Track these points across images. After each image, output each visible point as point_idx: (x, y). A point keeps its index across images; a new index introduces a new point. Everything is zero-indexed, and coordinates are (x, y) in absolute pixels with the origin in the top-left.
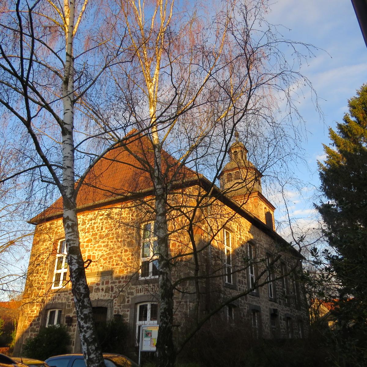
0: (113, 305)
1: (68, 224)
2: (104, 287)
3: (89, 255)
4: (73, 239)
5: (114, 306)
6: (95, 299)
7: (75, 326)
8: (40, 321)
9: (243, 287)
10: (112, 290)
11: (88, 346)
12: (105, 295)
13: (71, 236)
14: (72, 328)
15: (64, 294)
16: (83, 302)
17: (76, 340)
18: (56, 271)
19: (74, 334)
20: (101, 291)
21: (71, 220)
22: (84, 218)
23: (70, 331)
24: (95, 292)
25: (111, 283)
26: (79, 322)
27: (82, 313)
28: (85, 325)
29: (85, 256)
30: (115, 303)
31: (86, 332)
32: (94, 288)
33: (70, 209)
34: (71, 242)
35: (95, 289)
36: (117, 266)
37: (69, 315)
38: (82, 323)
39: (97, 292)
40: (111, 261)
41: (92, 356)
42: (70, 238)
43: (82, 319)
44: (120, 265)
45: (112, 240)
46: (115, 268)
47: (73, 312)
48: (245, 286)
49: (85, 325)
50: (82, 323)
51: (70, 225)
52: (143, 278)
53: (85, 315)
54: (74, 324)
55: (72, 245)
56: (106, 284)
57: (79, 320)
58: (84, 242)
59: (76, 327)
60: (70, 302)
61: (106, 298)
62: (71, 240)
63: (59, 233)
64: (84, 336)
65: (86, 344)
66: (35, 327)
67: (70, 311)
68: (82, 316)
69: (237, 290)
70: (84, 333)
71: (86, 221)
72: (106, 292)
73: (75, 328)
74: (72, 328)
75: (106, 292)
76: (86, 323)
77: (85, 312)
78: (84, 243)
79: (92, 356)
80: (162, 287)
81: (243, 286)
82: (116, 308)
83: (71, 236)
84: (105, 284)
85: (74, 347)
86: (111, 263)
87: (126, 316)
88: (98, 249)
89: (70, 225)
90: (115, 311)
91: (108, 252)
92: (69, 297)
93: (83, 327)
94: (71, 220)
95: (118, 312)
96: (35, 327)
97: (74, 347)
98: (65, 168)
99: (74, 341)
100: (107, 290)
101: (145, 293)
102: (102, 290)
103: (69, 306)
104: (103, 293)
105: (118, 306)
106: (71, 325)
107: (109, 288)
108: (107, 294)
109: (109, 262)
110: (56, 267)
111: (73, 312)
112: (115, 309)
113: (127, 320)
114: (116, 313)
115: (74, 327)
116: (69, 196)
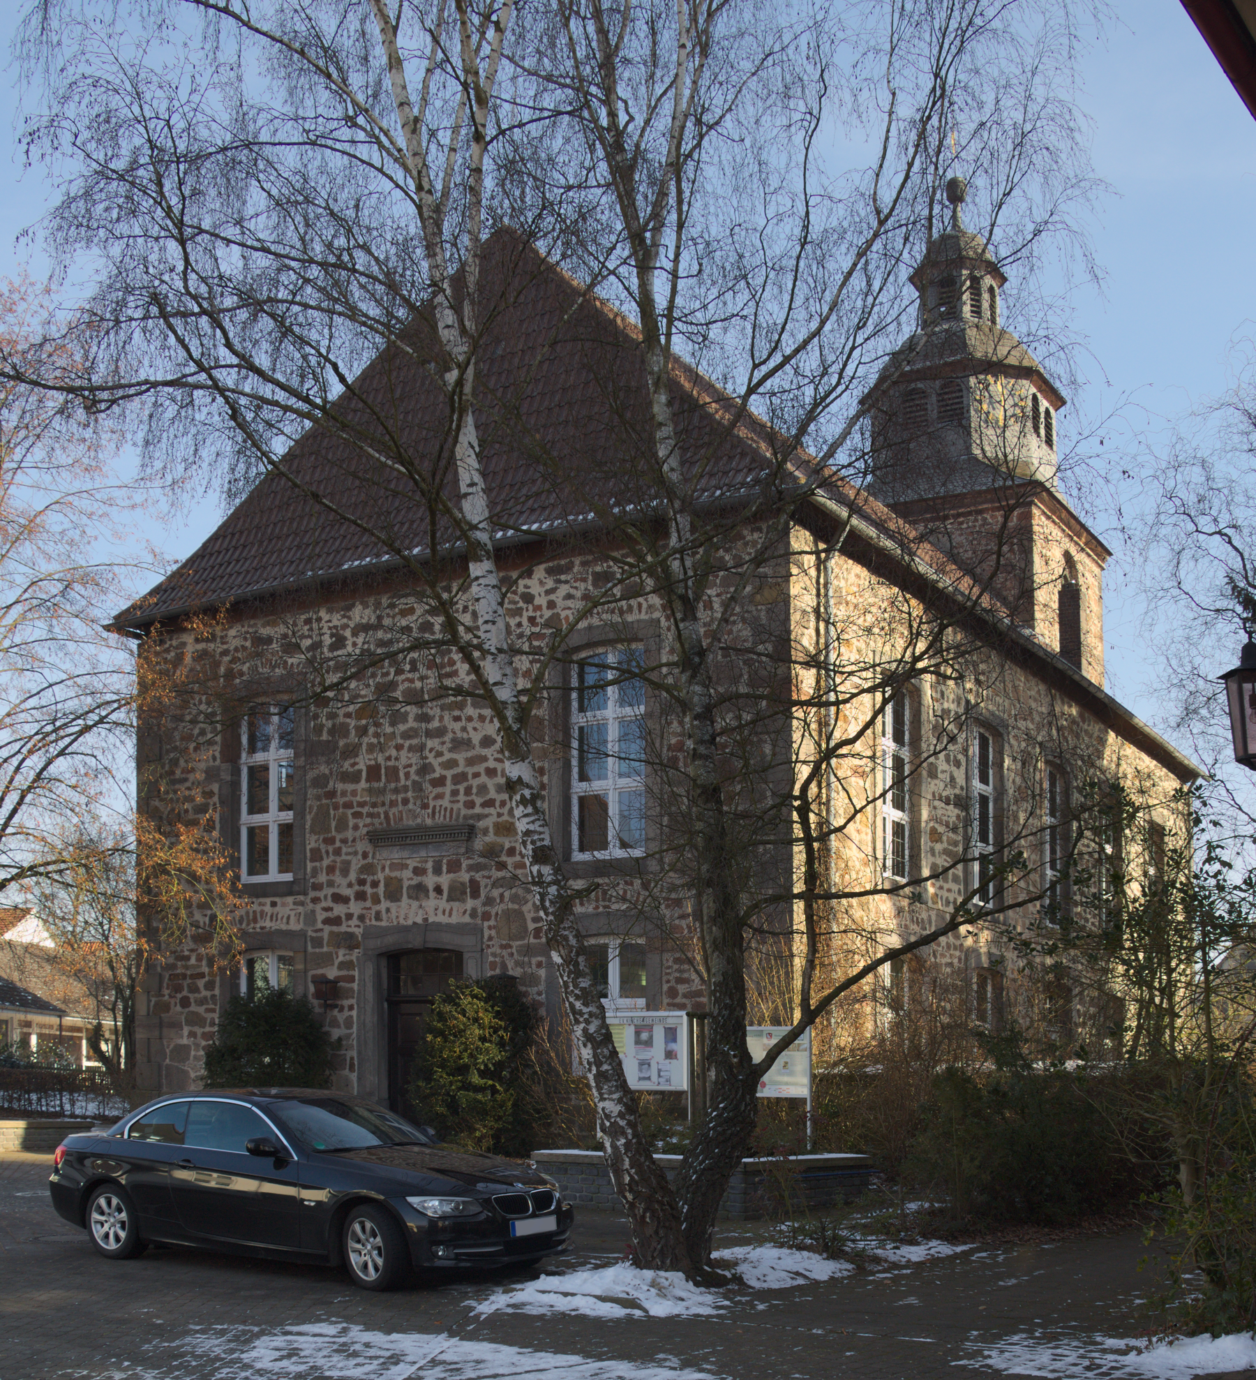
0: (482, 943)
1: (522, 796)
2: (445, 880)
3: (373, 762)
4: (538, 829)
5: (488, 946)
6: (415, 923)
7: (351, 1008)
8: (217, 992)
9: (949, 890)
10: (475, 894)
11: (594, 1048)
12: (451, 910)
13: (533, 822)
14: (341, 1017)
15: (295, 903)
16: (577, 964)
17: (359, 1053)
18: (247, 819)
19: (349, 1036)
20: (432, 894)
21: (528, 786)
22: (337, 620)
23: (334, 1023)
24: (410, 897)
25: (471, 868)
26: (571, 1004)
27: (576, 986)
28: (585, 1010)
29: (356, 767)
30: (490, 938)
31: (587, 1022)
32: (406, 884)
33: (523, 760)
34: (536, 837)
35: (409, 887)
36: (487, 810)
37: (320, 971)
38: (578, 1005)
39: (417, 899)
40: (461, 788)
41: (605, 1067)
42: (531, 827)
43: (577, 998)
44: (497, 804)
45: (456, 713)
46: (480, 817)
47: (336, 963)
48: (955, 887)
49: (585, 1010)
50: (578, 1005)
51: (528, 797)
52: (586, 856)
53: (583, 989)
54: (346, 1003)
55: (538, 844)
56: (449, 872)
57: (571, 1000)
58: (348, 715)
59: (354, 1013)
60: (321, 930)
61: (454, 920)
62: (535, 832)
63: (241, 674)
64: (585, 1031)
65: (589, 1045)
66: (201, 1010)
67: (327, 959)
68: (577, 992)
69: (926, 903)
70: (583, 1025)
71: (348, 633)
72: (450, 899)
73: (351, 1017)
74: (341, 1017)
75: (450, 899)
76: (586, 1004)
77: (583, 985)
78: (348, 720)
79: (605, 1067)
80: (713, 920)
81: (946, 886)
82: (494, 955)
83: (533, 822)
84: (444, 868)
85: (354, 1077)
86: (462, 797)
87: (534, 980)
88: (407, 744)
89: (528, 797)
90: (493, 965)
91: (448, 756)
92: (313, 912)
93: (581, 1013)
94: (528, 786)
95: (504, 966)
96: (201, 1010)
97: (354, 1077)
98: (492, 654)
99: (352, 1059)
100: (456, 893)
101: (597, 907)
102: (438, 890)
103: (318, 942)
104: (443, 903)
105: (503, 947)
106: (336, 1006)
107: (463, 884)
108: (455, 905)
109: (455, 793)
110: (244, 808)
111: (336, 963)
112: (491, 959)
113: (539, 994)
114: (498, 971)
115: (346, 1013)
116: (515, 727)
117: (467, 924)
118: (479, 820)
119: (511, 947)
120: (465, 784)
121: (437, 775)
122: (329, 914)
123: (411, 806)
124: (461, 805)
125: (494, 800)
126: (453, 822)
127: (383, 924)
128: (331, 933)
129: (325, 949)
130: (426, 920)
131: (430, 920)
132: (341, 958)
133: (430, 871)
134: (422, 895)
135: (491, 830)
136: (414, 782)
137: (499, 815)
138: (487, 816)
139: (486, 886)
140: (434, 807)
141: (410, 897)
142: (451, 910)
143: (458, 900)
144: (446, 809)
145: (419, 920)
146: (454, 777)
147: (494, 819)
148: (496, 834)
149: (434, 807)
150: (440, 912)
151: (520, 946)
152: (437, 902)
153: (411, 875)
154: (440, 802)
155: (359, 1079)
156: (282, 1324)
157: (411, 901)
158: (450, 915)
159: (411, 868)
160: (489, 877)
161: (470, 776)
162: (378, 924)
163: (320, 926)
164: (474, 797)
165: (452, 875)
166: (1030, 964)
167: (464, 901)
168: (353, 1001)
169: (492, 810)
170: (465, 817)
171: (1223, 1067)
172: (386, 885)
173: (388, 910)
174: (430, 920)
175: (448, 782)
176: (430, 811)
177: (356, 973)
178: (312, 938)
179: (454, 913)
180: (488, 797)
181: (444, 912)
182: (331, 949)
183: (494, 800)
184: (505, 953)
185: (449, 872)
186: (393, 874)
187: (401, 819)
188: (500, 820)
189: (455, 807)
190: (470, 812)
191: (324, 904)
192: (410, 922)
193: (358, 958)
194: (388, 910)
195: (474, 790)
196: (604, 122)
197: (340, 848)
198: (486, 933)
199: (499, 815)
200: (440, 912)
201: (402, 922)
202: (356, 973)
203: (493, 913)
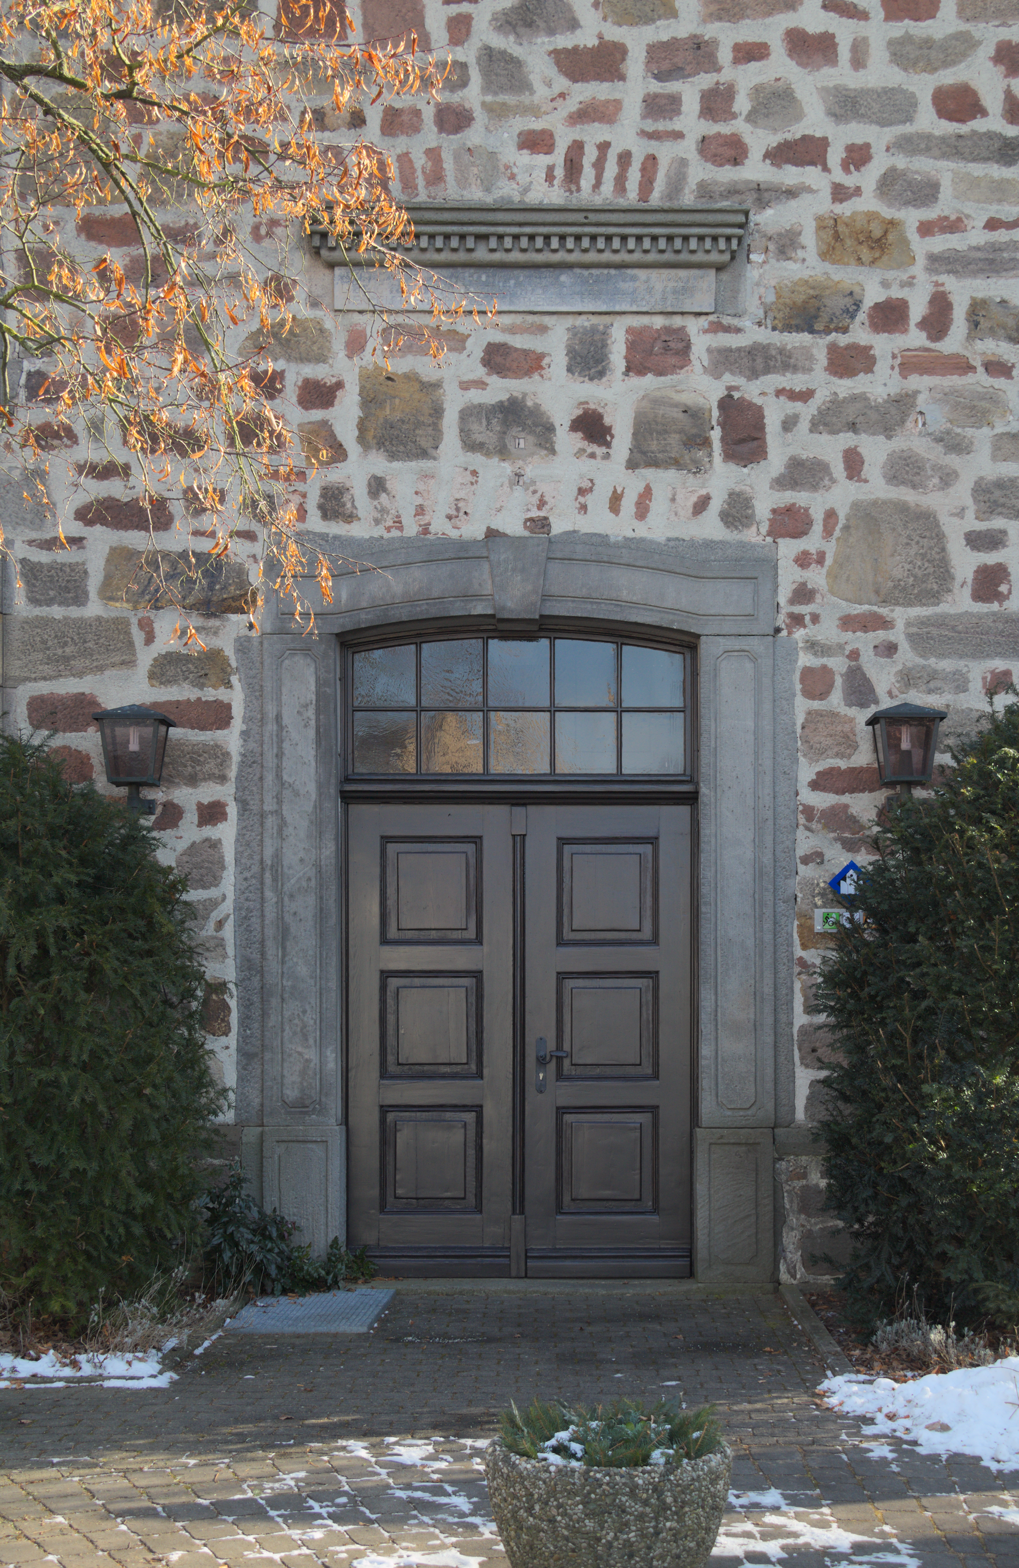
5: (797, 620)
6: (492, 534)
7: (212, 814)
12: (647, 494)
20: (567, 441)
30: (803, 594)
36: (791, 175)
39: (503, 452)
44: (835, 156)
47: (146, 657)
56: (634, 367)
60: (76, 541)
73: (214, 845)
112: (805, 660)
117: (709, 545)
118: (762, 204)
119: (885, 624)
120: (706, 80)
121: (586, 38)
122: (114, 488)
123: (474, 136)
124: (688, 148)
125: (824, 143)
126: (656, 199)
127: (360, 530)
128: (120, 556)
129: (94, 608)
130: (540, 525)
131: (558, 527)
132: (166, 641)
133: (558, 360)
134: (523, 442)
135: (809, 238)
136: (490, 56)
137: (840, 193)
138: (791, 193)
139: (789, 424)
140: (577, 148)
141: (471, 445)
142: (647, 494)
143: (677, 464)
144: (625, 159)
145: (512, 525)
146: (656, 52)
147: (822, 204)
148: (827, 254)
149: (577, 148)
150: (599, 500)
151: (923, 622)
152: (586, 467)
153: (480, 372)
154: (593, 134)
155: (247, 1056)
156: (43, 1452)
157: (477, 460)
158: (642, 511)
159: (476, 348)
160: (805, 396)
161: (725, 55)
162: (336, 528)
163: (65, 527)
164: (739, 126)
165: (649, 381)
166: (587, 1472)
167: (698, 469)
168: (225, 792)
169: (811, 175)
170: (704, 190)
171: (708, 1530)
172: (370, 401)
173: (377, 486)
174: (558, 527)
175: (635, 65)
176: (558, 158)
177: (236, 697)
178: (31, 571)
179: (658, 505)
180: (796, 131)
181: (615, 501)
182: (121, 609)
183: (824, 143)
184: (864, 642)
185: (634, 367)
186: (398, 366)
187: (436, 177)
188: (845, 209)
189: (666, 153)
190: (727, 174)
191: (87, 451)
192: (473, 530)
193: (243, 646)
194: (377, 486)
195: (742, 104)
196: (269, 852)
197: (162, 261)
198: (789, 576)
199: (840, 193)
200: (599, 500)
201: (440, 526)
202: (236, 697)
203: (818, 515)
